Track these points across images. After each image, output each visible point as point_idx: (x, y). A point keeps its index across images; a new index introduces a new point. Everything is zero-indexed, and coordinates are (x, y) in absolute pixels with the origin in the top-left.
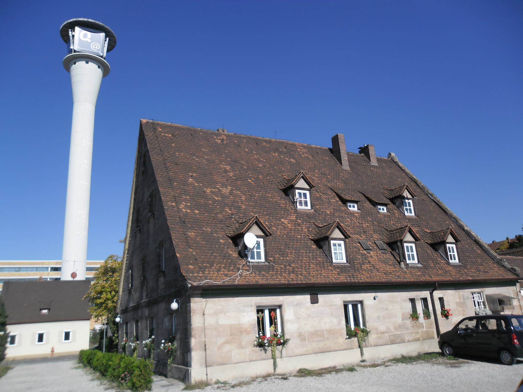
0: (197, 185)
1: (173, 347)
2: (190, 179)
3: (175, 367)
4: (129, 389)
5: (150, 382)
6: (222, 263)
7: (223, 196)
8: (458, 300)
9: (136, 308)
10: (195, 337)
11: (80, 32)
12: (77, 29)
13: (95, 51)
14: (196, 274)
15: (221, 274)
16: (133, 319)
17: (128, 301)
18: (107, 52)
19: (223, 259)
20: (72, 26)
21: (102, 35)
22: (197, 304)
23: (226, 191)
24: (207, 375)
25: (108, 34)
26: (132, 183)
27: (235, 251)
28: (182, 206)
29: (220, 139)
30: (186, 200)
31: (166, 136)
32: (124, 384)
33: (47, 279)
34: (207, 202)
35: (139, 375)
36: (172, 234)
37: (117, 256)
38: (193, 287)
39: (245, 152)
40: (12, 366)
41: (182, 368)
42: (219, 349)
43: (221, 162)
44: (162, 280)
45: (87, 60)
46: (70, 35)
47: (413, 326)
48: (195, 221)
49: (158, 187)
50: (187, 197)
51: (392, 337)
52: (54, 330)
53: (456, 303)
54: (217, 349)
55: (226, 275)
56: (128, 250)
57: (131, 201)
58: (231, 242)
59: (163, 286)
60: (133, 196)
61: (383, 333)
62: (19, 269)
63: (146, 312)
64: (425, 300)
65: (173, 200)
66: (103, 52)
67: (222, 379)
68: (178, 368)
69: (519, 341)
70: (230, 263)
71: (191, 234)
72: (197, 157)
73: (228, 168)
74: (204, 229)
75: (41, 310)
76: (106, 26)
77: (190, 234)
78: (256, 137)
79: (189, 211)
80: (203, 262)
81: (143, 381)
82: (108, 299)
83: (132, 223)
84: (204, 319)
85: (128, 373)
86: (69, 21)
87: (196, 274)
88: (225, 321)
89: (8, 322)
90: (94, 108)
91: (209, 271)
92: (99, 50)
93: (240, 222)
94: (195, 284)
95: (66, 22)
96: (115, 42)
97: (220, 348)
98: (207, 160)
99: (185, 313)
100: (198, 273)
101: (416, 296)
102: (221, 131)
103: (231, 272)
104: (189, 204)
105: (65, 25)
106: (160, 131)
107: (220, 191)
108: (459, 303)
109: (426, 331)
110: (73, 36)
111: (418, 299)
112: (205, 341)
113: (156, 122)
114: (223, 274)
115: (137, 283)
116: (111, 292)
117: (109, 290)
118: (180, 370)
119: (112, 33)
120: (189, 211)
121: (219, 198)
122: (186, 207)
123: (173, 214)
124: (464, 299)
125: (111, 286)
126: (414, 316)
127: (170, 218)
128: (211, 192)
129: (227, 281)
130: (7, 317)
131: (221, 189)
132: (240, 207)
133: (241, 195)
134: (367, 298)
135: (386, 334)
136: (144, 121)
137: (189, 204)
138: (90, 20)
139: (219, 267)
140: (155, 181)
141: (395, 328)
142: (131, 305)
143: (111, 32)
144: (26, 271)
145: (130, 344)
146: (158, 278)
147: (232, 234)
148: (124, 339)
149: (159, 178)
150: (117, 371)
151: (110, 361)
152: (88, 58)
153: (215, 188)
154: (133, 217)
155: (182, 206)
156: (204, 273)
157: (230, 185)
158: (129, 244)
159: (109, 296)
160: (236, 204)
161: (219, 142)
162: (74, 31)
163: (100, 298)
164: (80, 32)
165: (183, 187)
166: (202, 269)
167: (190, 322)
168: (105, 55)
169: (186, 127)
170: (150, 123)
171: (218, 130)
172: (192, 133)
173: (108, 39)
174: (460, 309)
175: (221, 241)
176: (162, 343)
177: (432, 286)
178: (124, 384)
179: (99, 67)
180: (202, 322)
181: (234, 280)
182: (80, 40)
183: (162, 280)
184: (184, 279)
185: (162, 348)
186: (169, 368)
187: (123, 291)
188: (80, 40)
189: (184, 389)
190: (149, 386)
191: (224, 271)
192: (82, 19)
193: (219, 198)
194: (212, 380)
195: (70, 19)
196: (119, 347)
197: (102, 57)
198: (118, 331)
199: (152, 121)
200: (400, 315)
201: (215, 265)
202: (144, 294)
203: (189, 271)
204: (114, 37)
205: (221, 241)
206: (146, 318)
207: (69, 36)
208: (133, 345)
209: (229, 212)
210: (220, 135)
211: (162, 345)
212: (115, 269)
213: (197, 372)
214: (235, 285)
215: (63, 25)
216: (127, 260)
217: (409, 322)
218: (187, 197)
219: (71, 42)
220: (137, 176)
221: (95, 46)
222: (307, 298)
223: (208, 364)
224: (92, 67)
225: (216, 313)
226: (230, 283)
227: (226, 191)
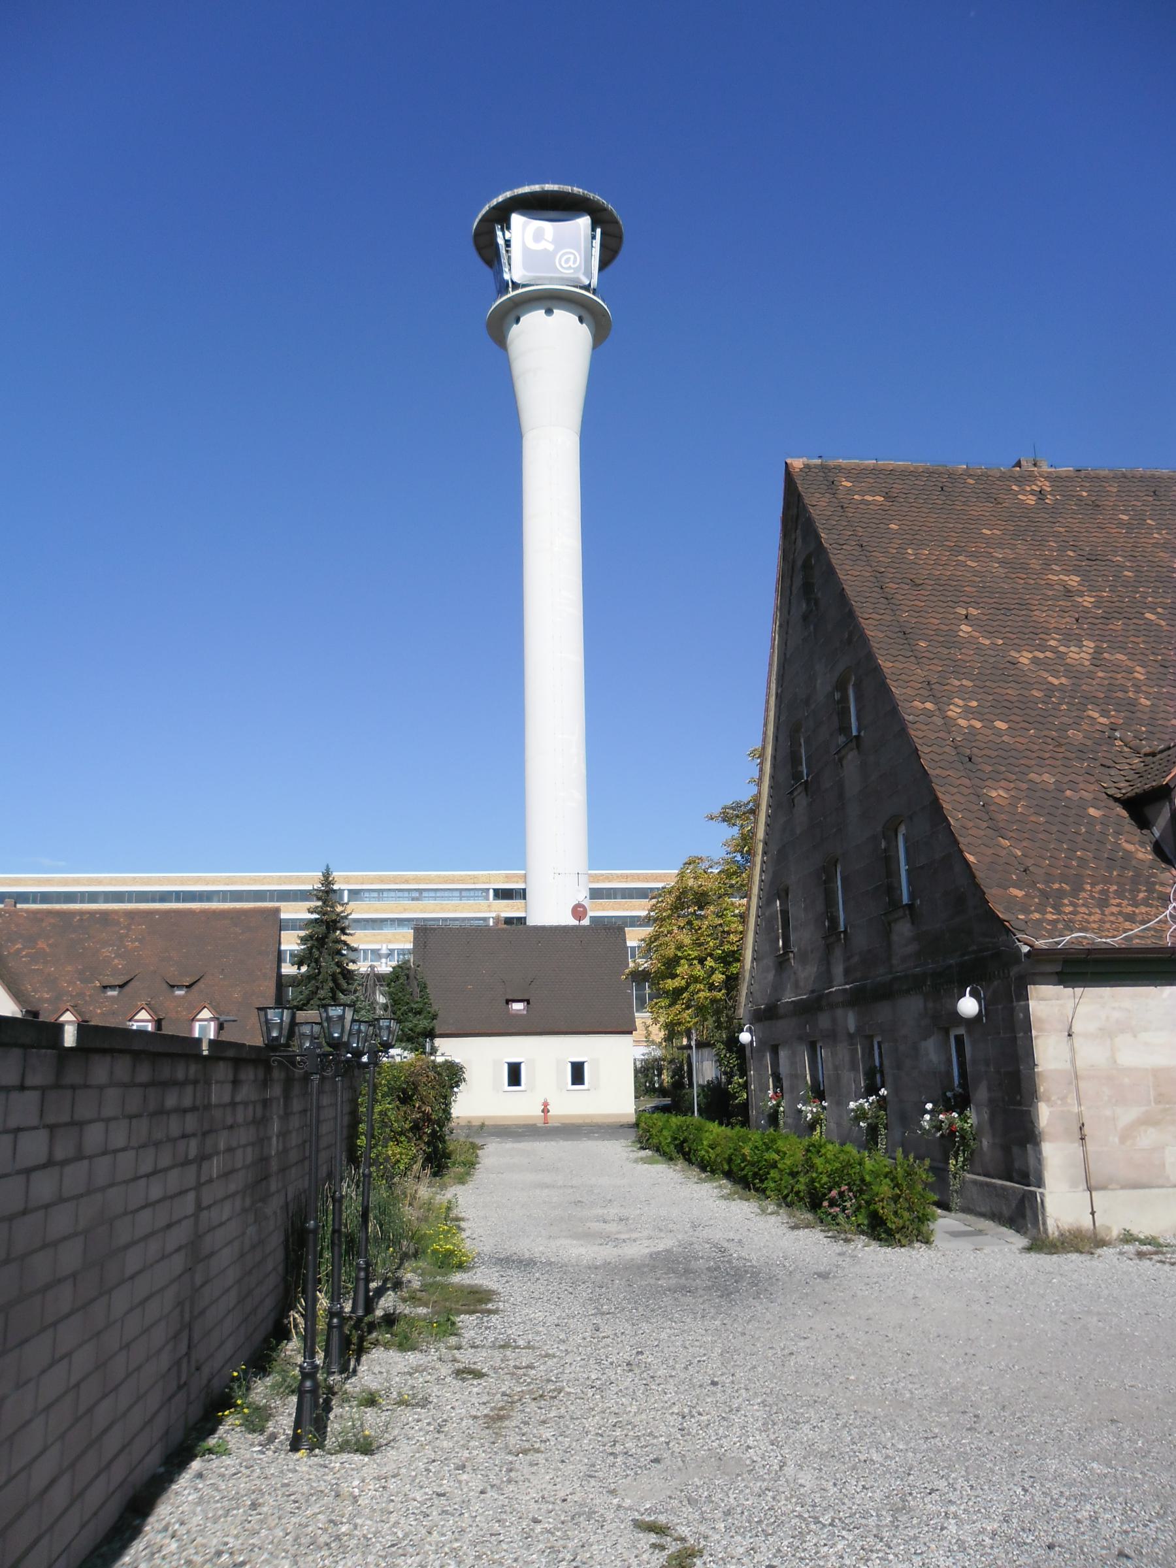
0: (987, 642)
2: (963, 627)
3: (975, 1182)
4: (863, 1233)
5: (923, 1219)
6: (1107, 881)
7: (1072, 672)
9: (809, 1008)
10: (1048, 1100)
11: (524, 226)
12: (516, 219)
14: (1037, 916)
15: (1113, 914)
16: (800, 1039)
17: (778, 987)
18: (601, 268)
19: (1110, 869)
20: (501, 216)
21: (517, 220)
22: (1047, 1003)
23: (1081, 654)
24: (1093, 1213)
25: (600, 217)
26: (768, 651)
27: (1142, 844)
28: (954, 711)
29: (1032, 492)
30: (962, 692)
31: (868, 503)
32: (841, 1218)
33: (485, 919)
34: (1023, 692)
35: (896, 1199)
36: (939, 794)
37: (709, 859)
38: (1036, 954)
39: (1121, 524)
40: (478, 1141)
41: (1003, 1188)
42: (1123, 1139)
43: (1047, 564)
44: (903, 929)
45: (549, 304)
46: (501, 241)
48: (1001, 753)
49: (870, 657)
50: (965, 682)
52: (546, 1055)
54: (1117, 1140)
55: (1130, 918)
56: (766, 843)
57: (767, 702)
58: (1125, 813)
59: (912, 948)
60: (773, 686)
62: (419, 895)
63: (850, 1020)
65: (927, 693)
66: (590, 277)
67: (1142, 1228)
68: (987, 1184)
70: (1135, 881)
71: (997, 793)
72: (971, 556)
73: (1073, 581)
74: (1032, 776)
75: (508, 1002)
76: (591, 195)
77: (994, 794)
78: (1148, 473)
79: (978, 725)
80: (1049, 878)
81: (906, 1215)
82: (696, 980)
83: (774, 766)
84: (1073, 1049)
85: (850, 1190)
86: (494, 202)
87: (1037, 916)
88: (1131, 1055)
89: (437, 1032)
90: (578, 439)
91: (1072, 904)
92: (577, 270)
93: (1147, 750)
94: (1041, 943)
95: (486, 208)
96: (619, 237)
97: (1127, 1135)
98: (1003, 562)
99: (1009, 1037)
100: (1044, 913)
102: (1027, 465)
103: (1143, 909)
104: (974, 704)
105: (484, 216)
106: (849, 489)
107: (1061, 656)
110: (508, 243)
112: (1080, 1115)
113: (831, 463)
114: (1120, 913)
115: (805, 936)
116: (702, 961)
117: (696, 954)
118: (1002, 1193)
119: (611, 213)
120: (978, 725)
121: (1063, 680)
122: (968, 712)
123: (933, 736)
125: (701, 945)
127: (926, 749)
128: (1035, 660)
129: (1137, 936)
130: (434, 1017)
131: (1062, 649)
132: (1133, 703)
133: (1130, 663)
136: (797, 463)
137: (974, 704)
138: (548, 187)
139: (1102, 892)
140: (864, 640)
142: (789, 998)
144: (435, 898)
145: (800, 1106)
146: (889, 924)
147: (1125, 790)
148: (771, 1092)
149: (873, 632)
150: (803, 1179)
151: (768, 1149)
152: (549, 300)
153: (1043, 648)
154: (775, 749)
155: (954, 711)
156: (1059, 913)
157: (1091, 637)
158: (767, 825)
159: (698, 971)
160: (1120, 694)
161: (1031, 500)
162: (509, 228)
163: (674, 976)
165: (946, 651)
166: (1052, 899)
167: (1031, 1054)
168: (594, 282)
169: (920, 465)
170: (816, 466)
171: (1019, 464)
172: (942, 484)
173: (599, 231)
175: (1092, 811)
176: (926, 1112)
178: (841, 1218)
179: (581, 320)
180: (1068, 1056)
181: (1159, 932)
183: (903, 929)
184: (1001, 928)
185: (926, 1125)
186: (955, 1185)
187: (754, 959)
188: (526, 250)
189: (1029, 1249)
190: (924, 1229)
191: (1119, 905)
192: (526, 189)
193: (1063, 680)
194: (1109, 1229)
195: (496, 196)
196: (753, 1113)
197: (587, 288)
198: (743, 1072)
199: (819, 461)
201: (1088, 887)
202: (838, 970)
203: (1011, 901)
204: (617, 222)
205: (1092, 811)
206: (851, 1037)
207: (497, 245)
208: (809, 1110)
209: (1102, 720)
210: (1030, 478)
211: (927, 1117)
212: (704, 894)
213: (1062, 1203)
214: (1164, 949)
215: (480, 216)
216: (762, 871)
218: (965, 682)
219: (504, 260)
220: (785, 627)
221: (567, 261)
223: (1093, 1183)
225: (1107, 1033)
226: (1149, 943)
227: (1081, 654)
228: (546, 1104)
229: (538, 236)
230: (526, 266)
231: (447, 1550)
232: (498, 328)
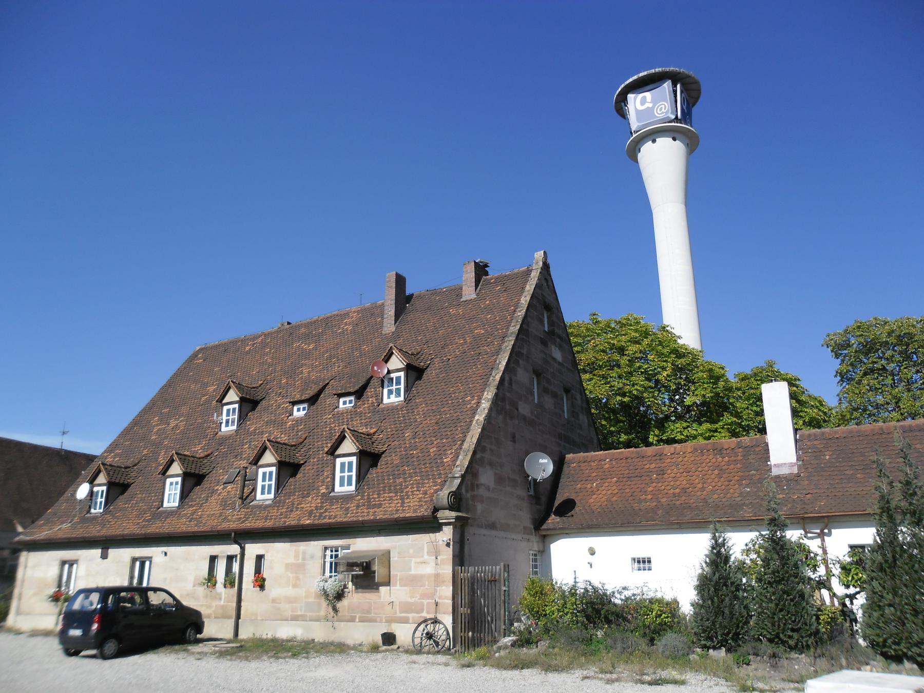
1: (222, 603)
8: (291, 560)
13: (662, 116)
20: (622, 99)
21: (631, 97)
25: (675, 78)
45: (653, 137)
47: (206, 597)
53: (287, 565)
64: (230, 559)
69: (98, 629)
76: (668, 69)
92: (667, 113)
101: (222, 552)
108: (293, 564)
109: (223, 606)
111: (223, 557)
124: (304, 559)
126: (211, 578)
134: (155, 552)
138: (641, 75)
143: (679, 73)
152: (652, 135)
164: (635, 99)
173: (678, 86)
174: (291, 575)
177: (242, 536)
179: (674, 139)
182: (636, 109)
192: (631, 80)
200: (191, 579)
221: (661, 109)
222: (98, 552)
224: (664, 142)
228: (400, 282)
229: (643, 101)
230: (638, 120)
231: (266, 671)
232: (633, 152)
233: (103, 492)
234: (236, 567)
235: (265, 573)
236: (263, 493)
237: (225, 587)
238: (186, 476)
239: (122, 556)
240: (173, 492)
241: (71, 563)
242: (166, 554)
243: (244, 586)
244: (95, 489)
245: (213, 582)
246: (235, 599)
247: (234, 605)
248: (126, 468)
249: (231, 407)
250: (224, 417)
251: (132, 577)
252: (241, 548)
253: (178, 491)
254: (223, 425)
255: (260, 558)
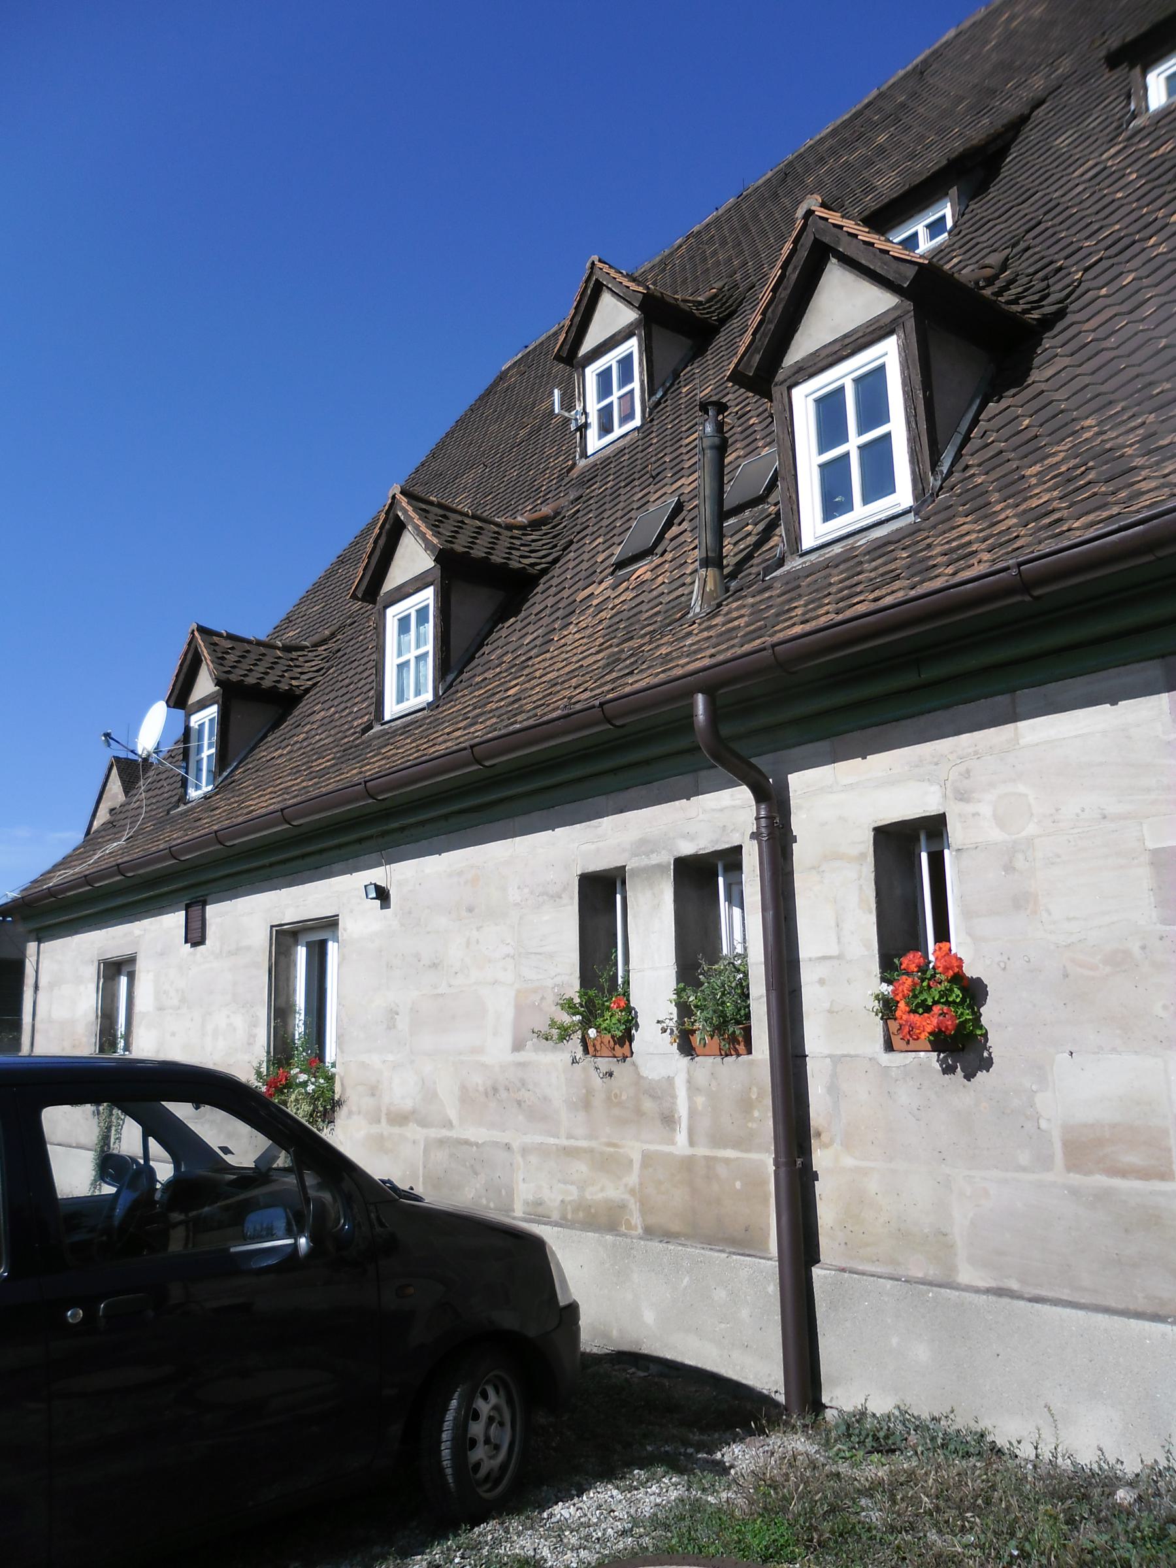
1: (680, 1144)
47: (586, 1103)
51: (440, 1156)
61: (400, 1119)
64: (700, 879)
101: (644, 845)
126: (599, 1005)
135: (414, 1132)
141: (466, 1097)
200: (501, 1006)
217: (557, 1068)
222: (175, 921)
233: (211, 720)
234: (743, 929)
235: (972, 941)
236: (833, 505)
237: (687, 1048)
238: (455, 571)
239: (246, 920)
240: (411, 656)
241: (316, 935)
242: (382, 895)
243: (816, 1040)
244: (195, 720)
245: (612, 1019)
246: (764, 1121)
247: (764, 1161)
248: (287, 649)
249: (611, 359)
250: (593, 406)
251: (280, 1012)
252: (761, 794)
253: (429, 647)
254: (592, 433)
255: (908, 852)
